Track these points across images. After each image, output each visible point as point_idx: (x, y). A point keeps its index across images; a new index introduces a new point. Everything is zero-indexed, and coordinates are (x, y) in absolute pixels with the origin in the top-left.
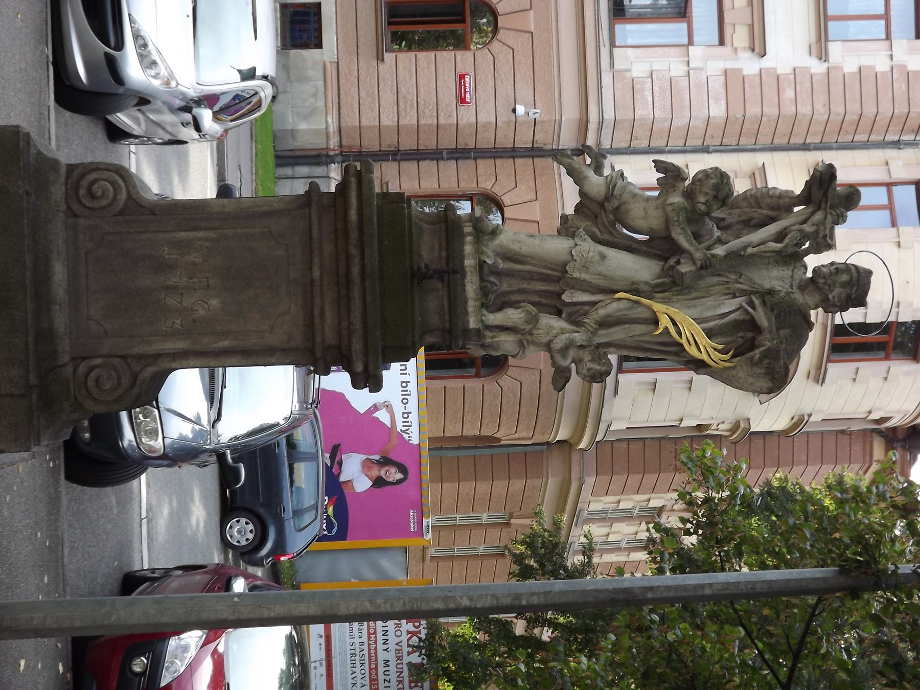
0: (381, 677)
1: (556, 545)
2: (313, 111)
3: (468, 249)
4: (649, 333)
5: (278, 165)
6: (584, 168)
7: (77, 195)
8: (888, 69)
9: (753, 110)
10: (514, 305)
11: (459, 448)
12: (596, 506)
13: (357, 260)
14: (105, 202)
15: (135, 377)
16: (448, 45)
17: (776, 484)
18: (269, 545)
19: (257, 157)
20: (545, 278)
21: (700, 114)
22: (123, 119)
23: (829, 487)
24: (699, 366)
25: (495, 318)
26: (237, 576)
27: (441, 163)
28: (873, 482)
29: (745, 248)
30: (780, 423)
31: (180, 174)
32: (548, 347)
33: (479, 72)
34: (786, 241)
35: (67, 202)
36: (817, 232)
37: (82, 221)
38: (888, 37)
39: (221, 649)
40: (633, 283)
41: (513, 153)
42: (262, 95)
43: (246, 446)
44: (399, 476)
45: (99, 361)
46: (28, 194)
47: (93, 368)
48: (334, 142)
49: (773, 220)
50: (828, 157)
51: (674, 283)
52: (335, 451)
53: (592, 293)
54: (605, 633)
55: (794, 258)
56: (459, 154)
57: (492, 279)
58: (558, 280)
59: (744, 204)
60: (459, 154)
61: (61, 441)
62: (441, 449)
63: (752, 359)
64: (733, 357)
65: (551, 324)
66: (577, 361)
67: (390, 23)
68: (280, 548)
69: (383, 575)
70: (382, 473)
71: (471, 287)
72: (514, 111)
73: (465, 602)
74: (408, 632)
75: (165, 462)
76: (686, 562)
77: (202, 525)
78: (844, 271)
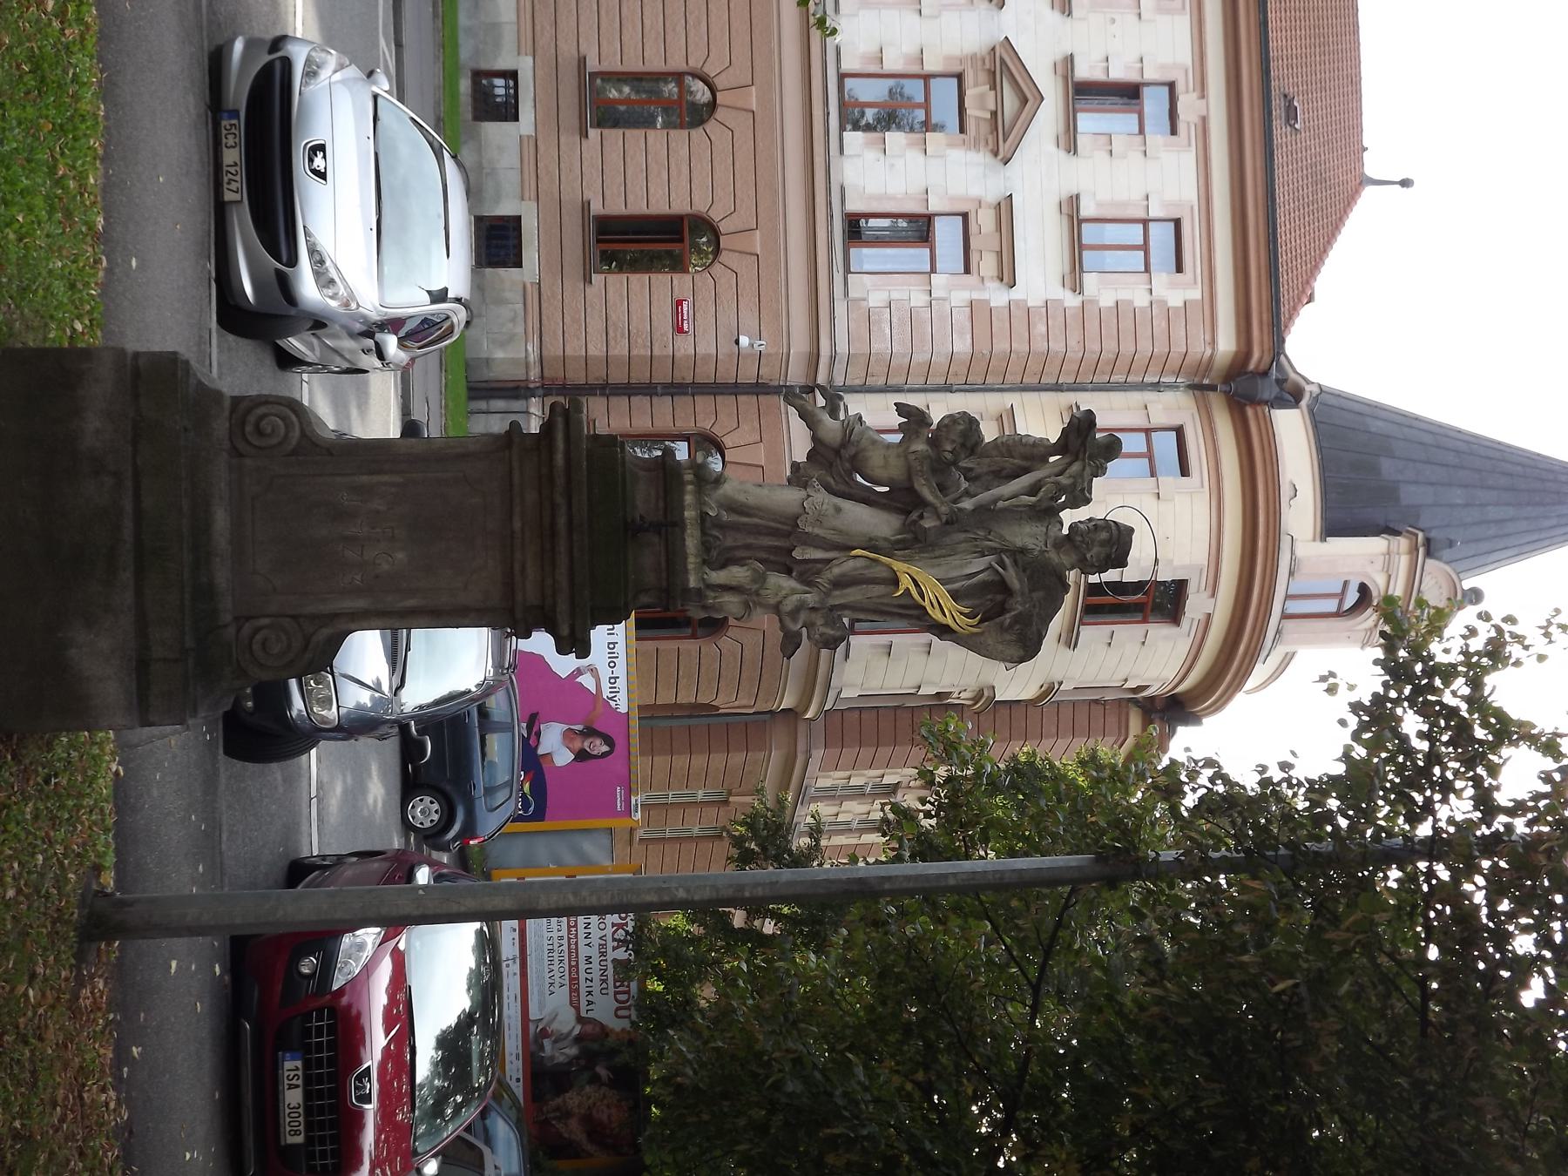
0: (583, 975)
1: (779, 827)
2: (511, 338)
3: (689, 499)
4: (889, 595)
5: (471, 398)
6: (818, 411)
7: (244, 435)
8: (1146, 304)
9: (1001, 346)
10: (739, 562)
11: (672, 717)
12: (824, 782)
13: (563, 510)
14: (274, 441)
15: (307, 641)
16: (664, 266)
17: (1023, 759)
18: (457, 827)
19: (447, 390)
20: (774, 533)
21: (943, 349)
22: (295, 344)
23: (1082, 763)
24: (943, 631)
25: (718, 577)
26: (420, 864)
27: (655, 399)
28: (1130, 758)
29: (995, 502)
30: (1029, 693)
31: (359, 407)
32: (777, 609)
33: (699, 297)
34: (1041, 494)
35: (231, 440)
36: (1074, 485)
37: (248, 462)
38: (1147, 270)
39: (402, 946)
40: (871, 539)
41: (736, 389)
42: (455, 320)
43: (433, 716)
44: (605, 748)
45: (266, 621)
46: (186, 430)
47: (258, 630)
48: (534, 374)
49: (1026, 471)
50: (1087, 401)
51: (916, 539)
52: (533, 721)
53: (826, 550)
54: (836, 926)
55: (1048, 513)
56: (675, 389)
57: (715, 533)
58: (788, 535)
59: (994, 453)
60: (675, 389)
61: (221, 712)
62: (652, 718)
63: (1001, 625)
64: (981, 621)
65: (780, 583)
66: (809, 625)
67: (598, 241)
68: (469, 830)
69: (588, 864)
70: (586, 745)
71: (692, 542)
72: (737, 342)
73: (681, 894)
74: (613, 925)
75: (340, 735)
76: (926, 849)
77: (380, 805)
78: (1103, 528)
